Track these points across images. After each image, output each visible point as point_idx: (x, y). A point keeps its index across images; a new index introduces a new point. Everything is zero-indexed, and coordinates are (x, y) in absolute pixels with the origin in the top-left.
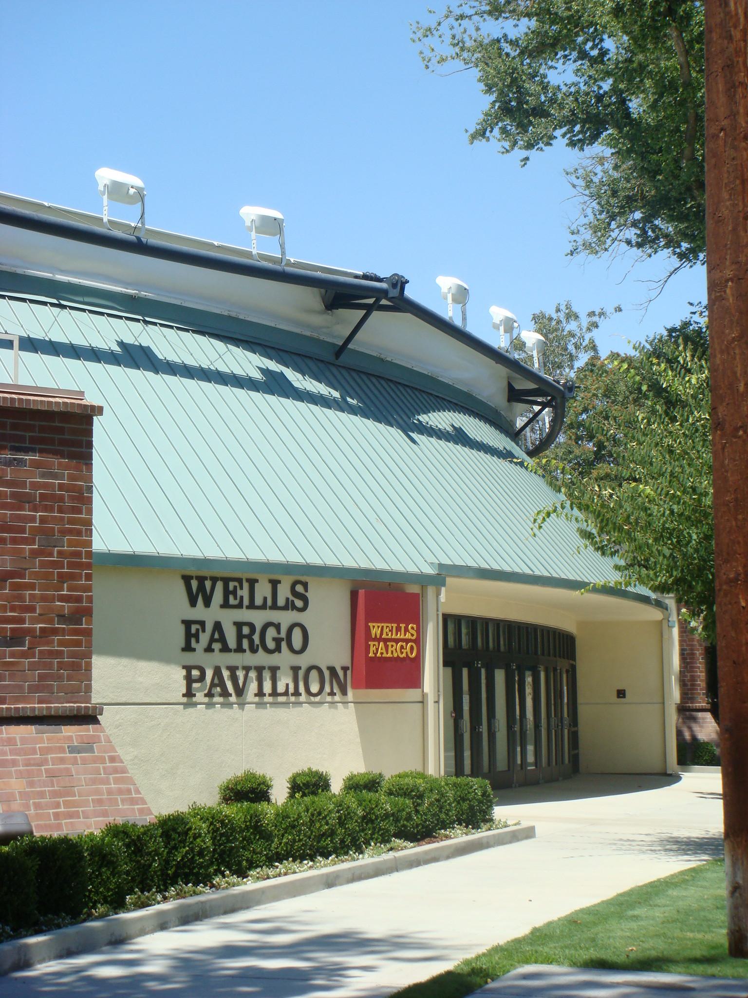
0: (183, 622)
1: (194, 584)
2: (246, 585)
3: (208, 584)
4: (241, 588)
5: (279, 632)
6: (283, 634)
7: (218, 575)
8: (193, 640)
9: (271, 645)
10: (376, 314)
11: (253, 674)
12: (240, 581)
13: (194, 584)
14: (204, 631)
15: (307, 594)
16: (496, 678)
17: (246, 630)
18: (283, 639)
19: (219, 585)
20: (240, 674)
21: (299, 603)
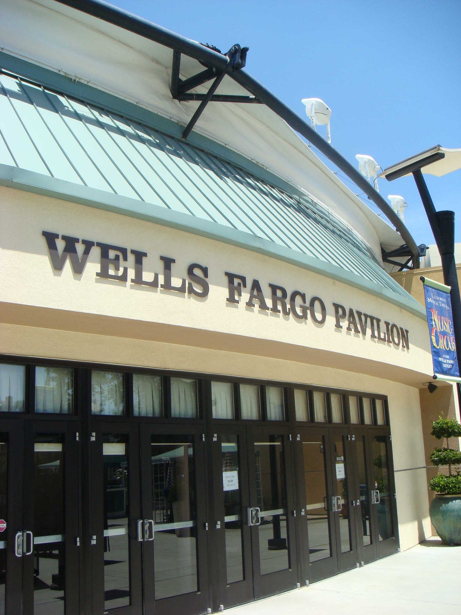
0: (227, 274)
1: (60, 244)
2: (131, 258)
3: (80, 248)
4: (125, 259)
5: (304, 302)
6: (308, 304)
7: (95, 239)
8: (236, 293)
9: (299, 311)
10: (211, 105)
11: (369, 320)
12: (124, 251)
13: (60, 244)
14: (245, 286)
15: (206, 280)
16: (260, 541)
17: (279, 293)
18: (307, 308)
19: (96, 252)
20: (363, 318)
21: (198, 289)
